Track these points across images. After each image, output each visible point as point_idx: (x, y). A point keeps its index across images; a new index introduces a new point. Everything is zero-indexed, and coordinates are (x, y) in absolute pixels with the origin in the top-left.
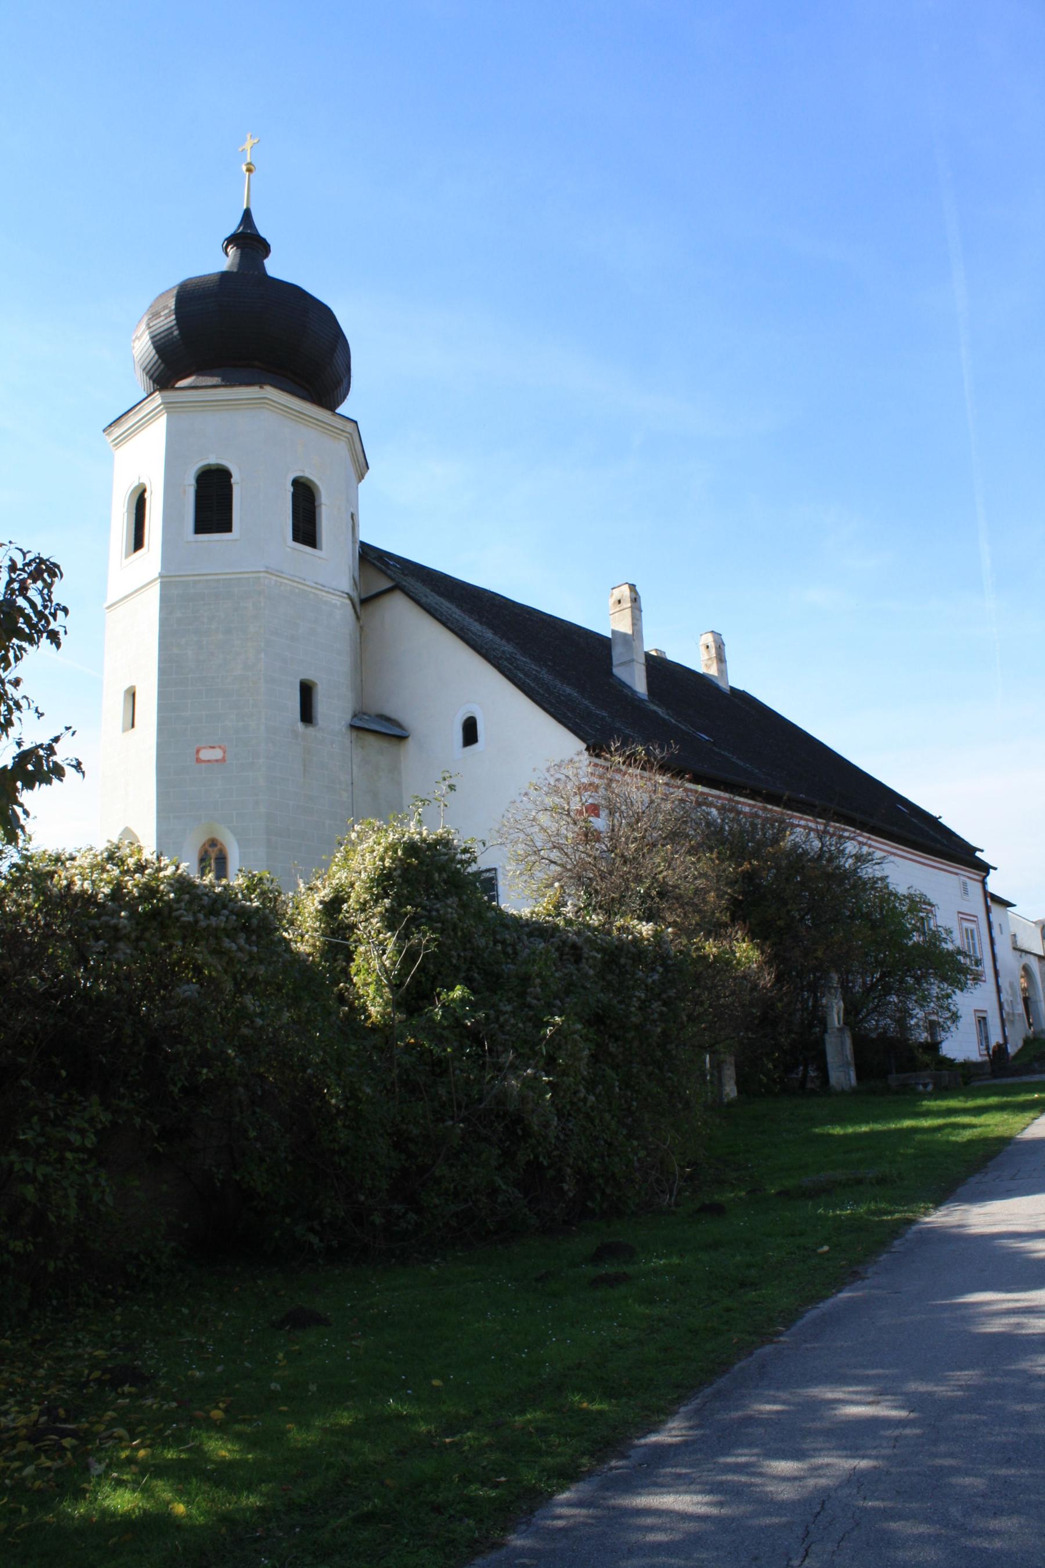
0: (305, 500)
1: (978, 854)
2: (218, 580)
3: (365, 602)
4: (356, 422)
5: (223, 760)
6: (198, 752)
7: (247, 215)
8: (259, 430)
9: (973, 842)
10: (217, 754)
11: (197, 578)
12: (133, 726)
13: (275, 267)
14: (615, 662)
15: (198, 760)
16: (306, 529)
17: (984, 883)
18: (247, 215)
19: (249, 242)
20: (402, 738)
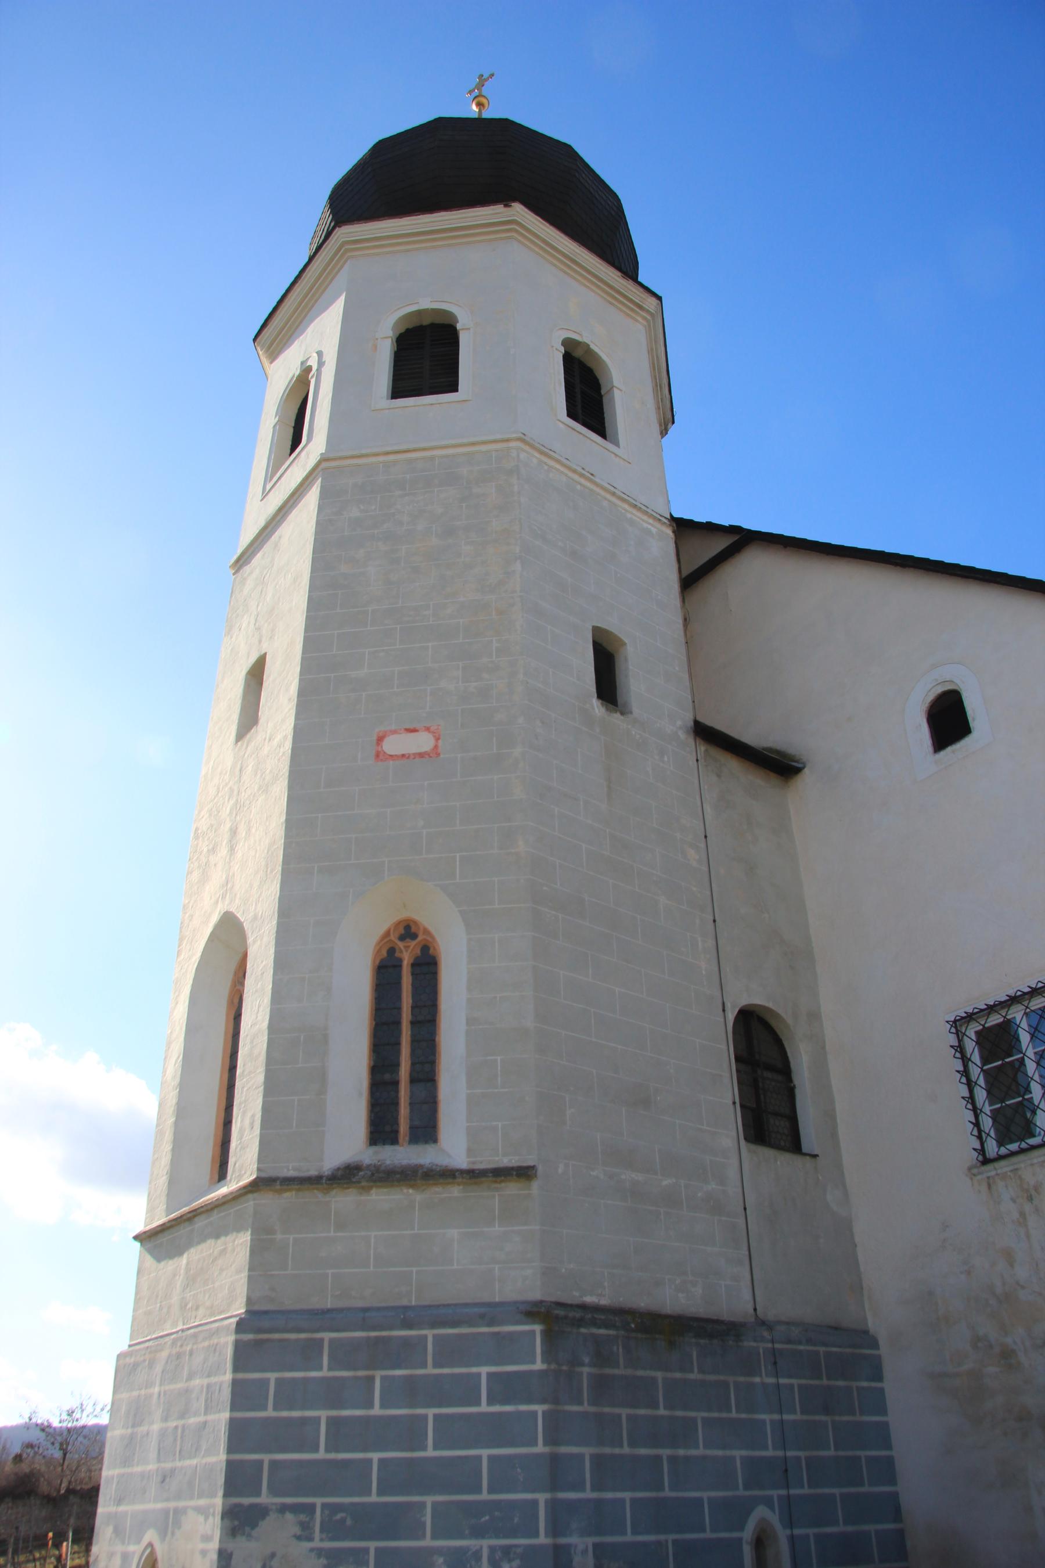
2: (432, 458)
4: (660, 298)
5: (435, 751)
6: (380, 739)
10: (423, 742)
11: (392, 457)
20: (797, 771)
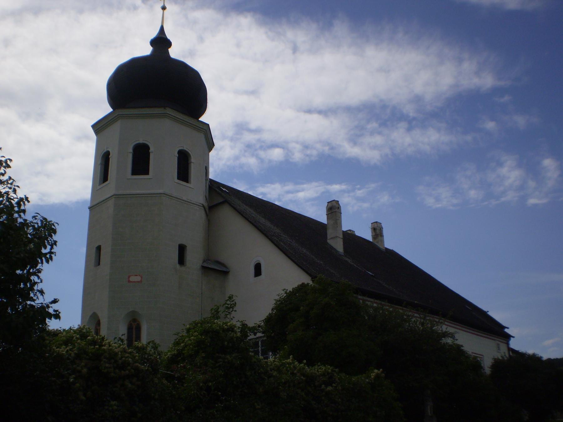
0: (184, 159)
1: (506, 330)
3: (211, 209)
5: (141, 281)
6: (129, 277)
7: (162, 29)
8: (162, 133)
9: (504, 324)
10: (138, 279)
12: (99, 264)
13: (174, 53)
14: (329, 237)
15: (129, 281)
16: (184, 174)
17: (508, 344)
18: (162, 29)
19: (161, 42)
